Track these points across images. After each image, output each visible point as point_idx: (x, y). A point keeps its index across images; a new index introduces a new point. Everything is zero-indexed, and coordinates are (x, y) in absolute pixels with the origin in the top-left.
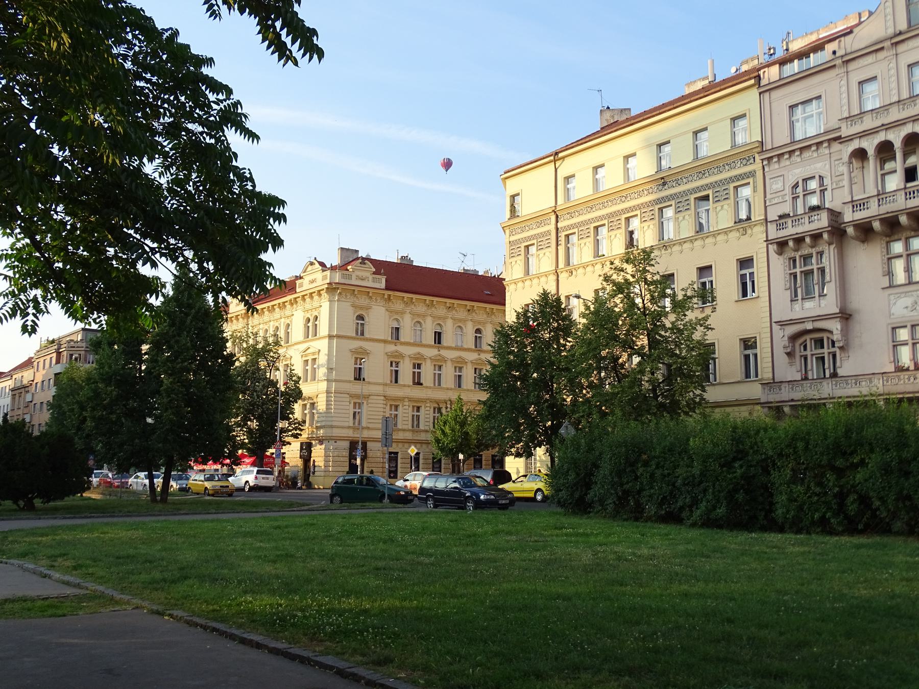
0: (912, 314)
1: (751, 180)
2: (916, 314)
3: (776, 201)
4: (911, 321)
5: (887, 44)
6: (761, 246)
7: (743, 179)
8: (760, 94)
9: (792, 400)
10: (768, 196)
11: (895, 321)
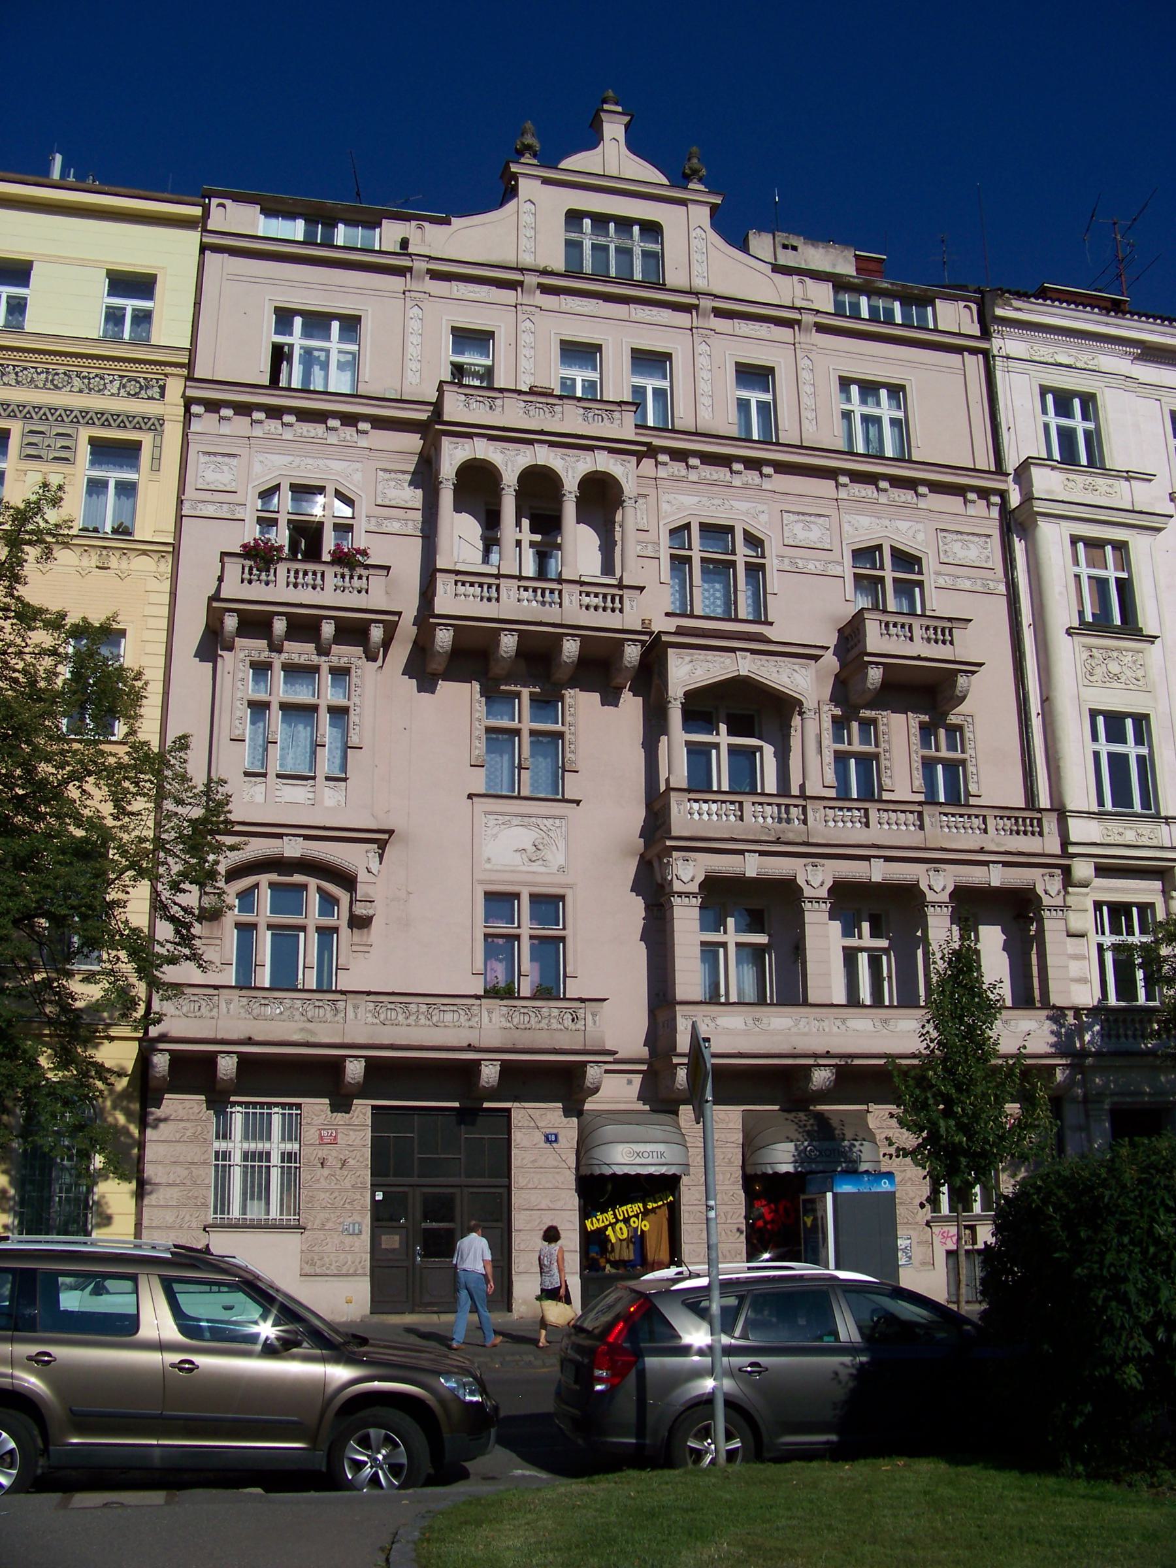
0: (535, 867)
1: (146, 439)
2: (542, 869)
3: (210, 511)
4: (491, 882)
5: (531, 280)
6: (154, 610)
7: (122, 426)
8: (203, 248)
9: (249, 1041)
10: (190, 493)
11: (495, 877)
